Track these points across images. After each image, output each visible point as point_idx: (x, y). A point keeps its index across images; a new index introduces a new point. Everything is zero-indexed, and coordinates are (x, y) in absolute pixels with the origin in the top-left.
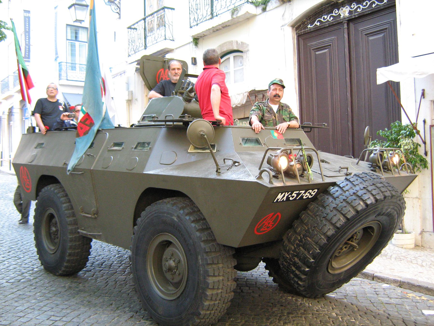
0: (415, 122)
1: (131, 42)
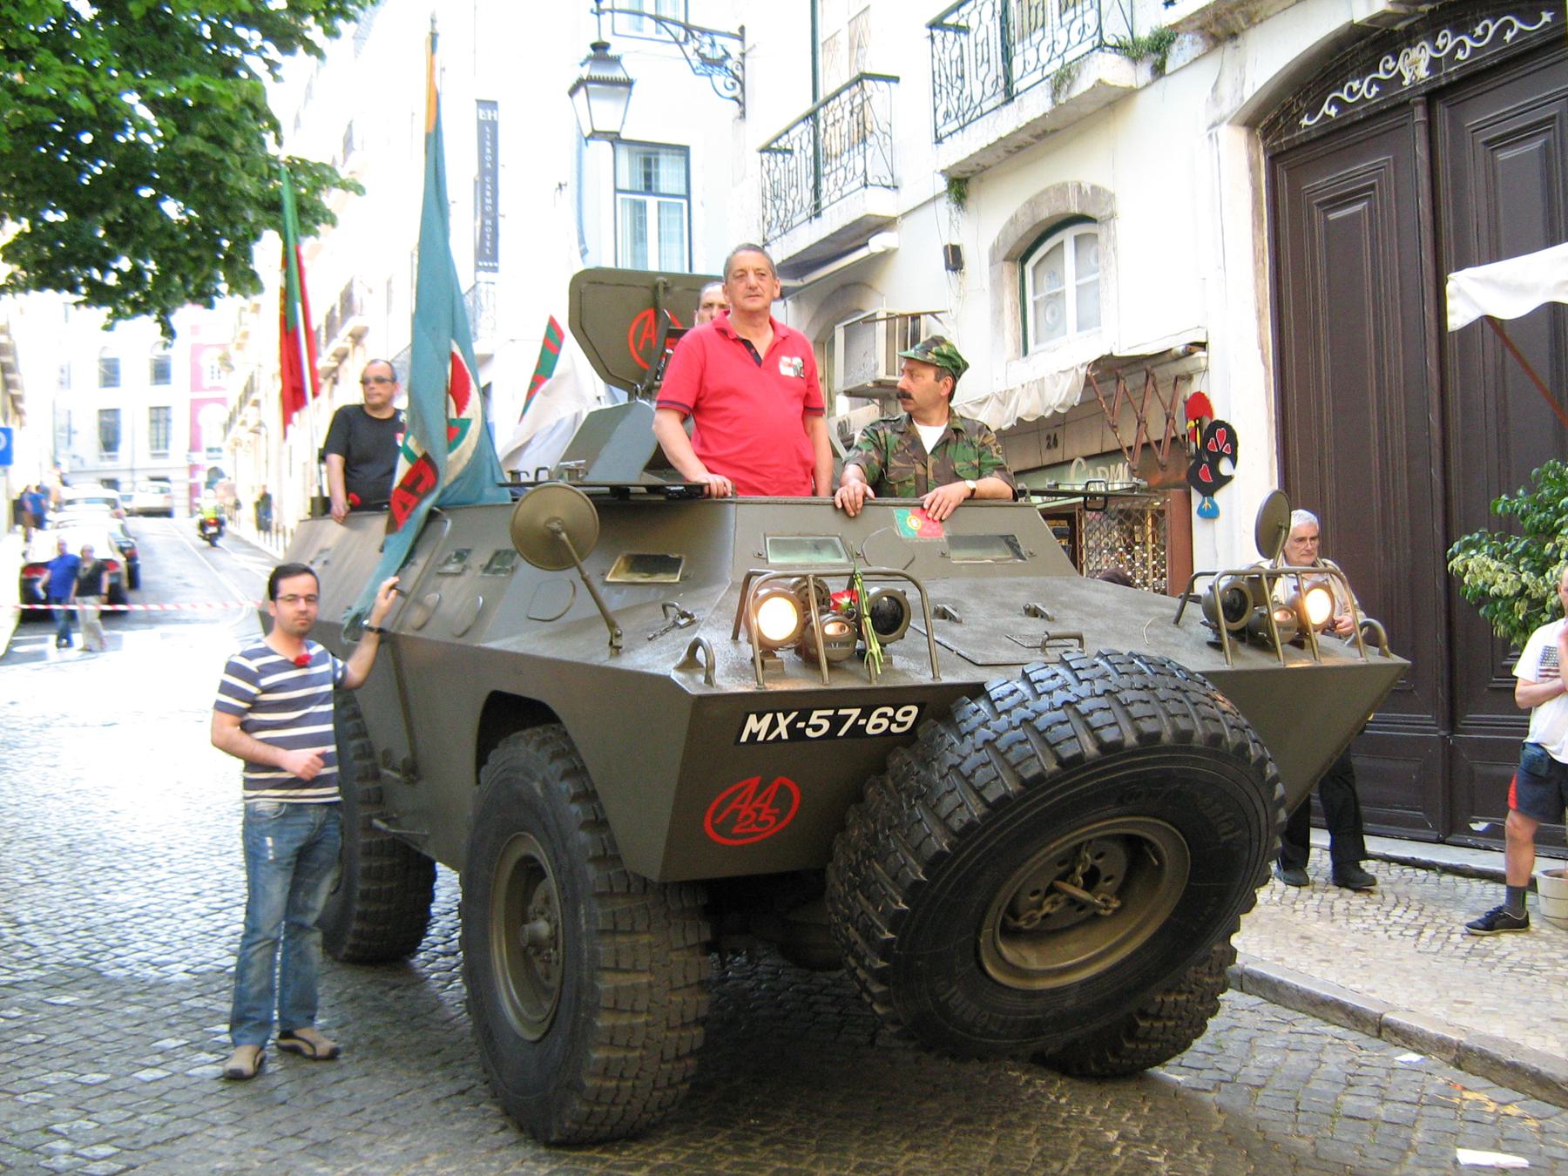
1: (773, 195)
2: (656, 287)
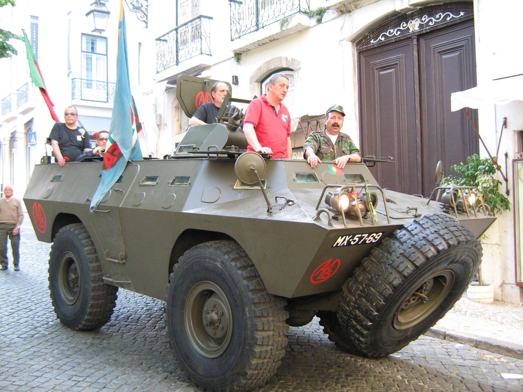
0: (495, 156)
1: (161, 56)
2: (205, 83)
